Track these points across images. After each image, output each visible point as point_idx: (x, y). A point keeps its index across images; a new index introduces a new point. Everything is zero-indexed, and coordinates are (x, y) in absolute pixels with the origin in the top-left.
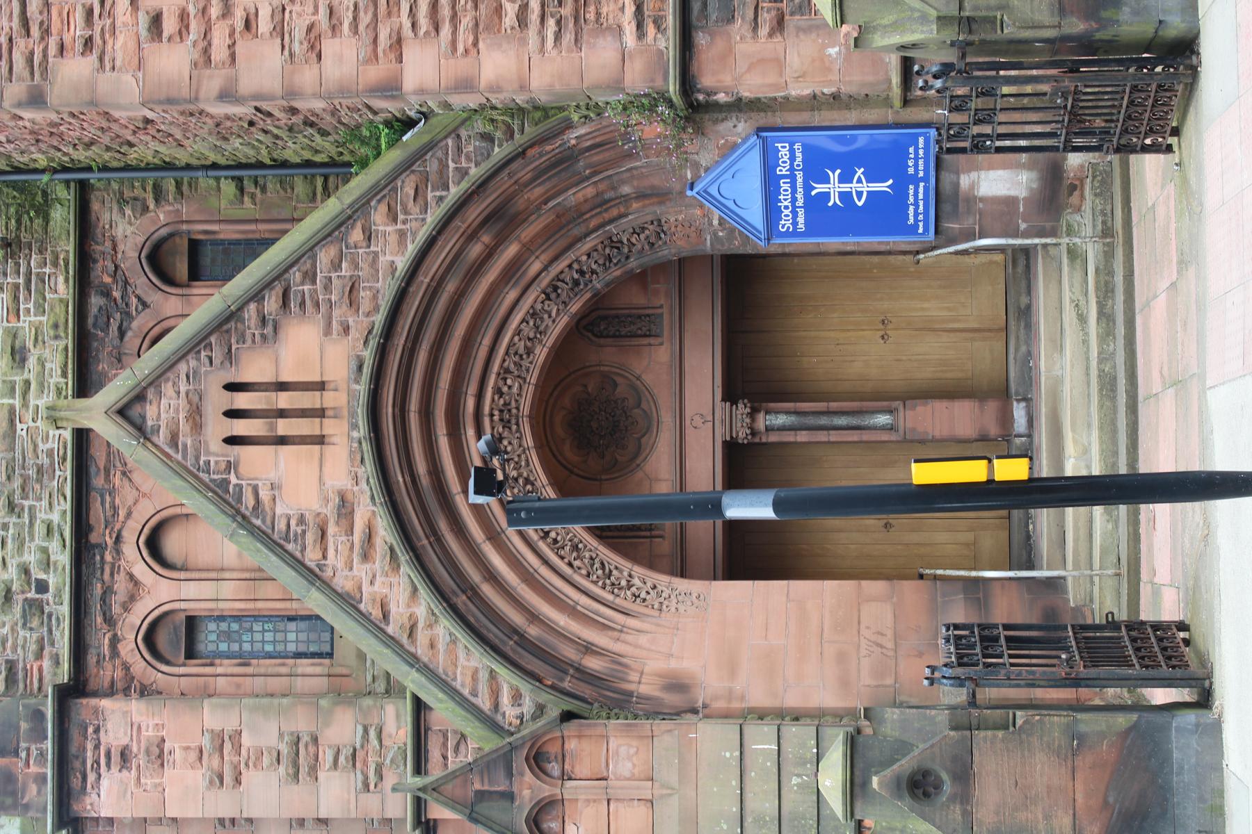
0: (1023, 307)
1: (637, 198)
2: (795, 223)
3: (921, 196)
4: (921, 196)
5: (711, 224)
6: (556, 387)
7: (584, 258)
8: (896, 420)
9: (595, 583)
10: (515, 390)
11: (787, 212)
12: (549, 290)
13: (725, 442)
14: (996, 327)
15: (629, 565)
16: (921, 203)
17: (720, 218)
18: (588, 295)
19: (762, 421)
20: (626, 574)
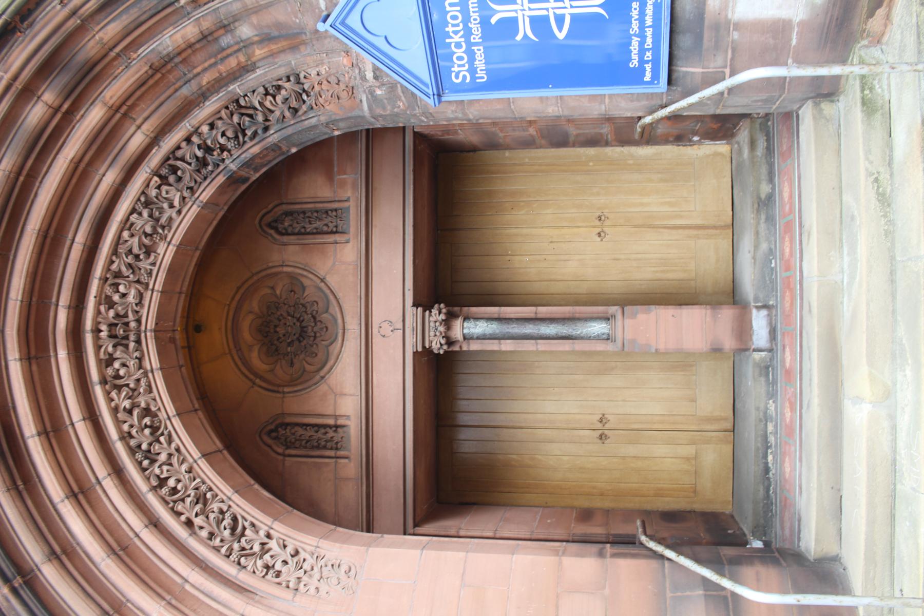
0: (763, 196)
1: (260, 42)
2: (473, 71)
3: (649, 21)
4: (649, 21)
5: (364, 78)
6: (239, 288)
7: (205, 129)
8: (613, 328)
9: (217, 549)
10: (131, 299)
11: (460, 52)
12: (164, 172)
13: (415, 354)
14: (722, 224)
15: (268, 520)
16: (649, 32)
17: (375, 69)
18: (221, 179)
19: (459, 329)
20: (262, 533)
